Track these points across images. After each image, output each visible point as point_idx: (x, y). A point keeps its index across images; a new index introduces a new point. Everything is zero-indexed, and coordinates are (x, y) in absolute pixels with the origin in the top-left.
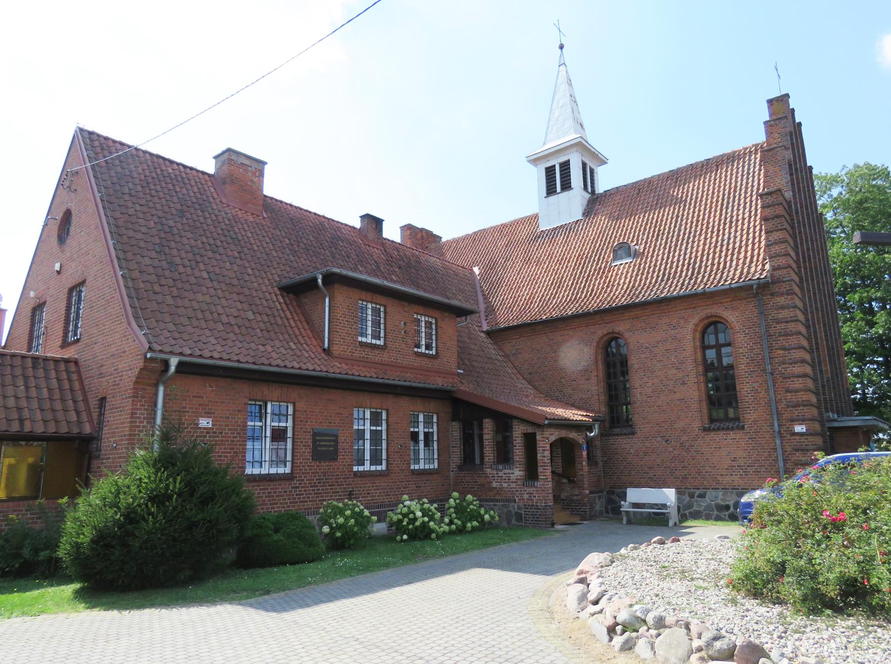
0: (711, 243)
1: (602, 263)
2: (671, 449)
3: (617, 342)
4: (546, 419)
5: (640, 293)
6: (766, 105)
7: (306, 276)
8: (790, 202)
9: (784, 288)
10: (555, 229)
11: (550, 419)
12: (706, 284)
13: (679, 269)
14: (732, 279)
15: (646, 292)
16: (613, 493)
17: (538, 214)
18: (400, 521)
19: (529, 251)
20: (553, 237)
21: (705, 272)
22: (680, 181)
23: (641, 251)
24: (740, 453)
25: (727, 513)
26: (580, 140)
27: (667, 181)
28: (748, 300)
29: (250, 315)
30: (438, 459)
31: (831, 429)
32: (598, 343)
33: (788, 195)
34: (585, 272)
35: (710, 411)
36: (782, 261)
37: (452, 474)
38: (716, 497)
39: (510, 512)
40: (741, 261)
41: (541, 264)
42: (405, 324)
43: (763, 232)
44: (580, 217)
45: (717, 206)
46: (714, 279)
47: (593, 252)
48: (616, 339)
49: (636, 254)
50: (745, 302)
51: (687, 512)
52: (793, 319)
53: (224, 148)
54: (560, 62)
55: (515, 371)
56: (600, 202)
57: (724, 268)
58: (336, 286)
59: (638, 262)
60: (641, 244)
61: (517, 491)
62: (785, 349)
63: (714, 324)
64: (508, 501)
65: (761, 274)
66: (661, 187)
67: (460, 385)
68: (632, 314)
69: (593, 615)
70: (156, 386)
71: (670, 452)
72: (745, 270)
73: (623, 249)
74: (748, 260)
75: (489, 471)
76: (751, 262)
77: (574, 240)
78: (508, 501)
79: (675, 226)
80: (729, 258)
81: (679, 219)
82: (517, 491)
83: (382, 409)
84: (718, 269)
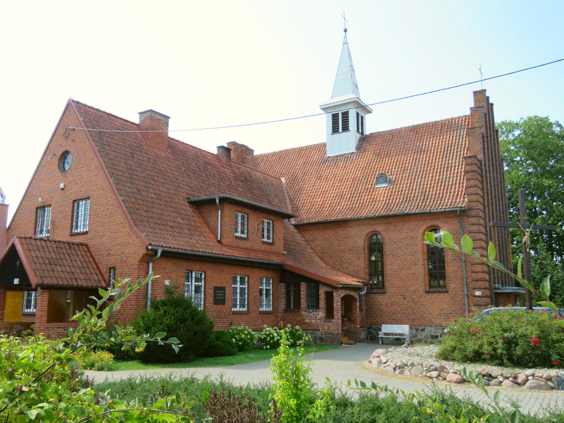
0: (435, 180)
2: (406, 303)
3: (377, 237)
4: (340, 284)
5: (393, 208)
6: (472, 94)
8: (481, 161)
9: (474, 213)
10: (338, 156)
11: (342, 284)
12: (431, 207)
13: (416, 195)
14: (446, 205)
15: (396, 208)
16: (371, 328)
18: (265, 338)
19: (320, 171)
20: (336, 162)
21: (431, 198)
22: (419, 134)
23: (394, 179)
27: (410, 132)
28: (455, 218)
29: (179, 220)
30: (273, 305)
32: (366, 237)
33: (480, 157)
34: (358, 190)
35: (430, 281)
36: (474, 198)
37: (280, 314)
38: (431, 331)
39: (316, 336)
40: (452, 194)
41: (328, 181)
42: (258, 225)
43: (465, 180)
44: (354, 150)
45: (440, 155)
46: (436, 204)
47: (363, 176)
48: (377, 235)
49: (390, 182)
50: (452, 219)
51: (414, 339)
52: (478, 231)
54: (344, 41)
55: (312, 251)
56: (367, 141)
57: (442, 197)
58: (225, 204)
59: (392, 187)
60: (393, 175)
61: (321, 325)
64: (315, 330)
65: (462, 204)
66: (407, 136)
67: (286, 261)
68: (387, 221)
69: (384, 367)
70: (148, 263)
72: (454, 200)
73: (382, 178)
74: (456, 193)
75: (303, 313)
76: (457, 195)
78: (315, 330)
80: (445, 191)
81: (417, 161)
82: (321, 325)
83: (245, 275)
84: (439, 197)
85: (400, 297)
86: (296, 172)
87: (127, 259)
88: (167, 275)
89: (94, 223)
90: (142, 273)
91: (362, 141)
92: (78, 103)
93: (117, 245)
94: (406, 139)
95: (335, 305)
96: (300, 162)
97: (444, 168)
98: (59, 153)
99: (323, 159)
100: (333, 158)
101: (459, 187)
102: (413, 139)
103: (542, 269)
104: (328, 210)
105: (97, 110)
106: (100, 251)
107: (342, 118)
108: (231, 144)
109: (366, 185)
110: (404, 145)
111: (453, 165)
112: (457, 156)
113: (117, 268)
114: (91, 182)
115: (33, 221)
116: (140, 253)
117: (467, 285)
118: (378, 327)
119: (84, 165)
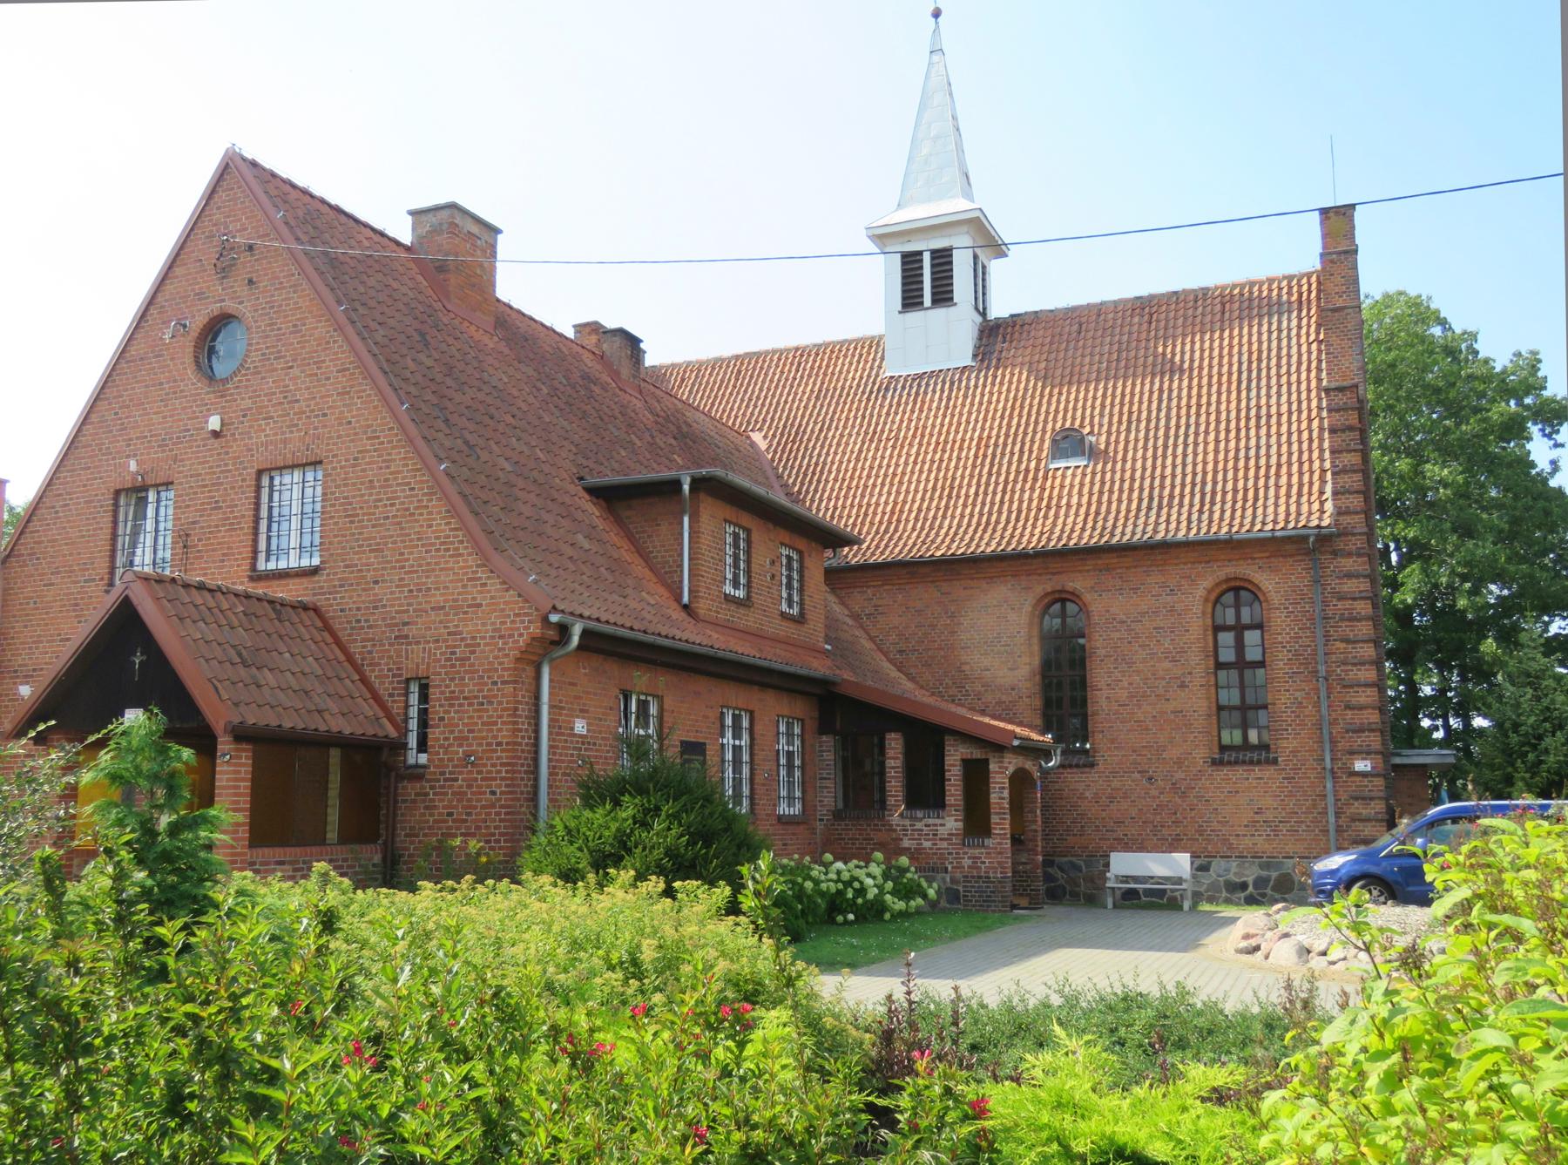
1: (1029, 460)
2: (1154, 793)
7: (666, 474)
10: (921, 376)
17: (881, 337)
22: (1158, 321)
23: (1102, 447)
24: (1269, 801)
25: (1242, 895)
26: (978, 214)
27: (1132, 316)
31: (1396, 767)
37: (819, 826)
38: (1227, 870)
44: (969, 362)
45: (1229, 382)
47: (1007, 436)
48: (1063, 601)
49: (1093, 453)
53: (442, 200)
54: (933, 44)
56: (1004, 337)
60: (1099, 434)
62: (1347, 641)
63: (1239, 590)
66: (1122, 326)
68: (1100, 562)
71: (1154, 797)
73: (1069, 442)
76: (1300, 495)
77: (963, 405)
79: (1159, 410)
85: (1137, 775)
86: (795, 417)
87: (473, 652)
88: (578, 704)
89: (339, 542)
90: (523, 696)
91: (989, 336)
92: (254, 164)
93: (432, 609)
94: (1121, 334)
95: (994, 798)
96: (806, 390)
97: (1248, 419)
98: (197, 322)
99: (874, 383)
100: (906, 380)
101: (1301, 474)
102: (1144, 335)
103: (1538, 699)
104: (914, 529)
105: (305, 192)
106: (370, 627)
107: (933, 266)
108: (588, 330)
109: (1020, 461)
110: (1119, 351)
111: (1274, 410)
112: (1280, 386)
113: (435, 681)
114: (325, 415)
115: (106, 533)
116: (521, 635)
117: (1333, 742)
118: (1071, 862)
119: (294, 360)
